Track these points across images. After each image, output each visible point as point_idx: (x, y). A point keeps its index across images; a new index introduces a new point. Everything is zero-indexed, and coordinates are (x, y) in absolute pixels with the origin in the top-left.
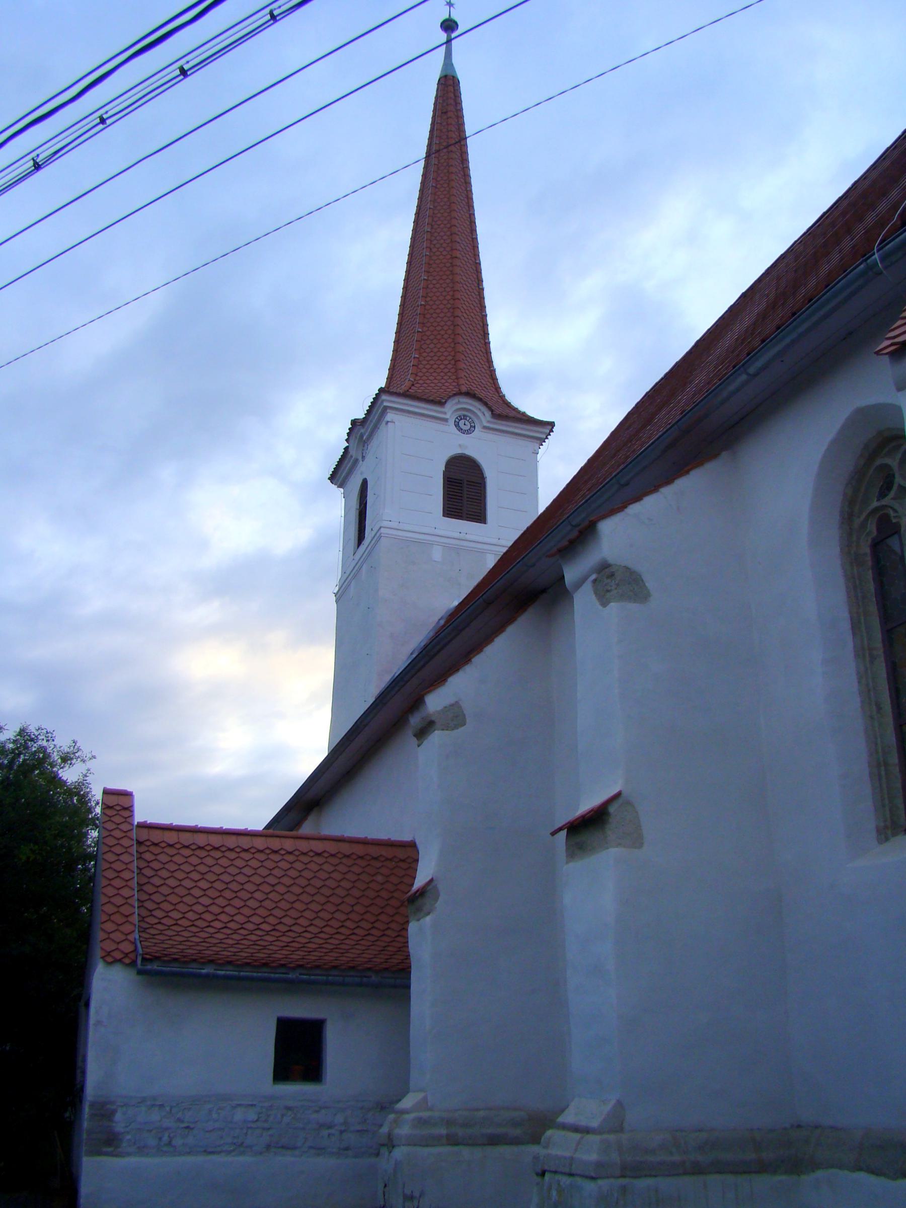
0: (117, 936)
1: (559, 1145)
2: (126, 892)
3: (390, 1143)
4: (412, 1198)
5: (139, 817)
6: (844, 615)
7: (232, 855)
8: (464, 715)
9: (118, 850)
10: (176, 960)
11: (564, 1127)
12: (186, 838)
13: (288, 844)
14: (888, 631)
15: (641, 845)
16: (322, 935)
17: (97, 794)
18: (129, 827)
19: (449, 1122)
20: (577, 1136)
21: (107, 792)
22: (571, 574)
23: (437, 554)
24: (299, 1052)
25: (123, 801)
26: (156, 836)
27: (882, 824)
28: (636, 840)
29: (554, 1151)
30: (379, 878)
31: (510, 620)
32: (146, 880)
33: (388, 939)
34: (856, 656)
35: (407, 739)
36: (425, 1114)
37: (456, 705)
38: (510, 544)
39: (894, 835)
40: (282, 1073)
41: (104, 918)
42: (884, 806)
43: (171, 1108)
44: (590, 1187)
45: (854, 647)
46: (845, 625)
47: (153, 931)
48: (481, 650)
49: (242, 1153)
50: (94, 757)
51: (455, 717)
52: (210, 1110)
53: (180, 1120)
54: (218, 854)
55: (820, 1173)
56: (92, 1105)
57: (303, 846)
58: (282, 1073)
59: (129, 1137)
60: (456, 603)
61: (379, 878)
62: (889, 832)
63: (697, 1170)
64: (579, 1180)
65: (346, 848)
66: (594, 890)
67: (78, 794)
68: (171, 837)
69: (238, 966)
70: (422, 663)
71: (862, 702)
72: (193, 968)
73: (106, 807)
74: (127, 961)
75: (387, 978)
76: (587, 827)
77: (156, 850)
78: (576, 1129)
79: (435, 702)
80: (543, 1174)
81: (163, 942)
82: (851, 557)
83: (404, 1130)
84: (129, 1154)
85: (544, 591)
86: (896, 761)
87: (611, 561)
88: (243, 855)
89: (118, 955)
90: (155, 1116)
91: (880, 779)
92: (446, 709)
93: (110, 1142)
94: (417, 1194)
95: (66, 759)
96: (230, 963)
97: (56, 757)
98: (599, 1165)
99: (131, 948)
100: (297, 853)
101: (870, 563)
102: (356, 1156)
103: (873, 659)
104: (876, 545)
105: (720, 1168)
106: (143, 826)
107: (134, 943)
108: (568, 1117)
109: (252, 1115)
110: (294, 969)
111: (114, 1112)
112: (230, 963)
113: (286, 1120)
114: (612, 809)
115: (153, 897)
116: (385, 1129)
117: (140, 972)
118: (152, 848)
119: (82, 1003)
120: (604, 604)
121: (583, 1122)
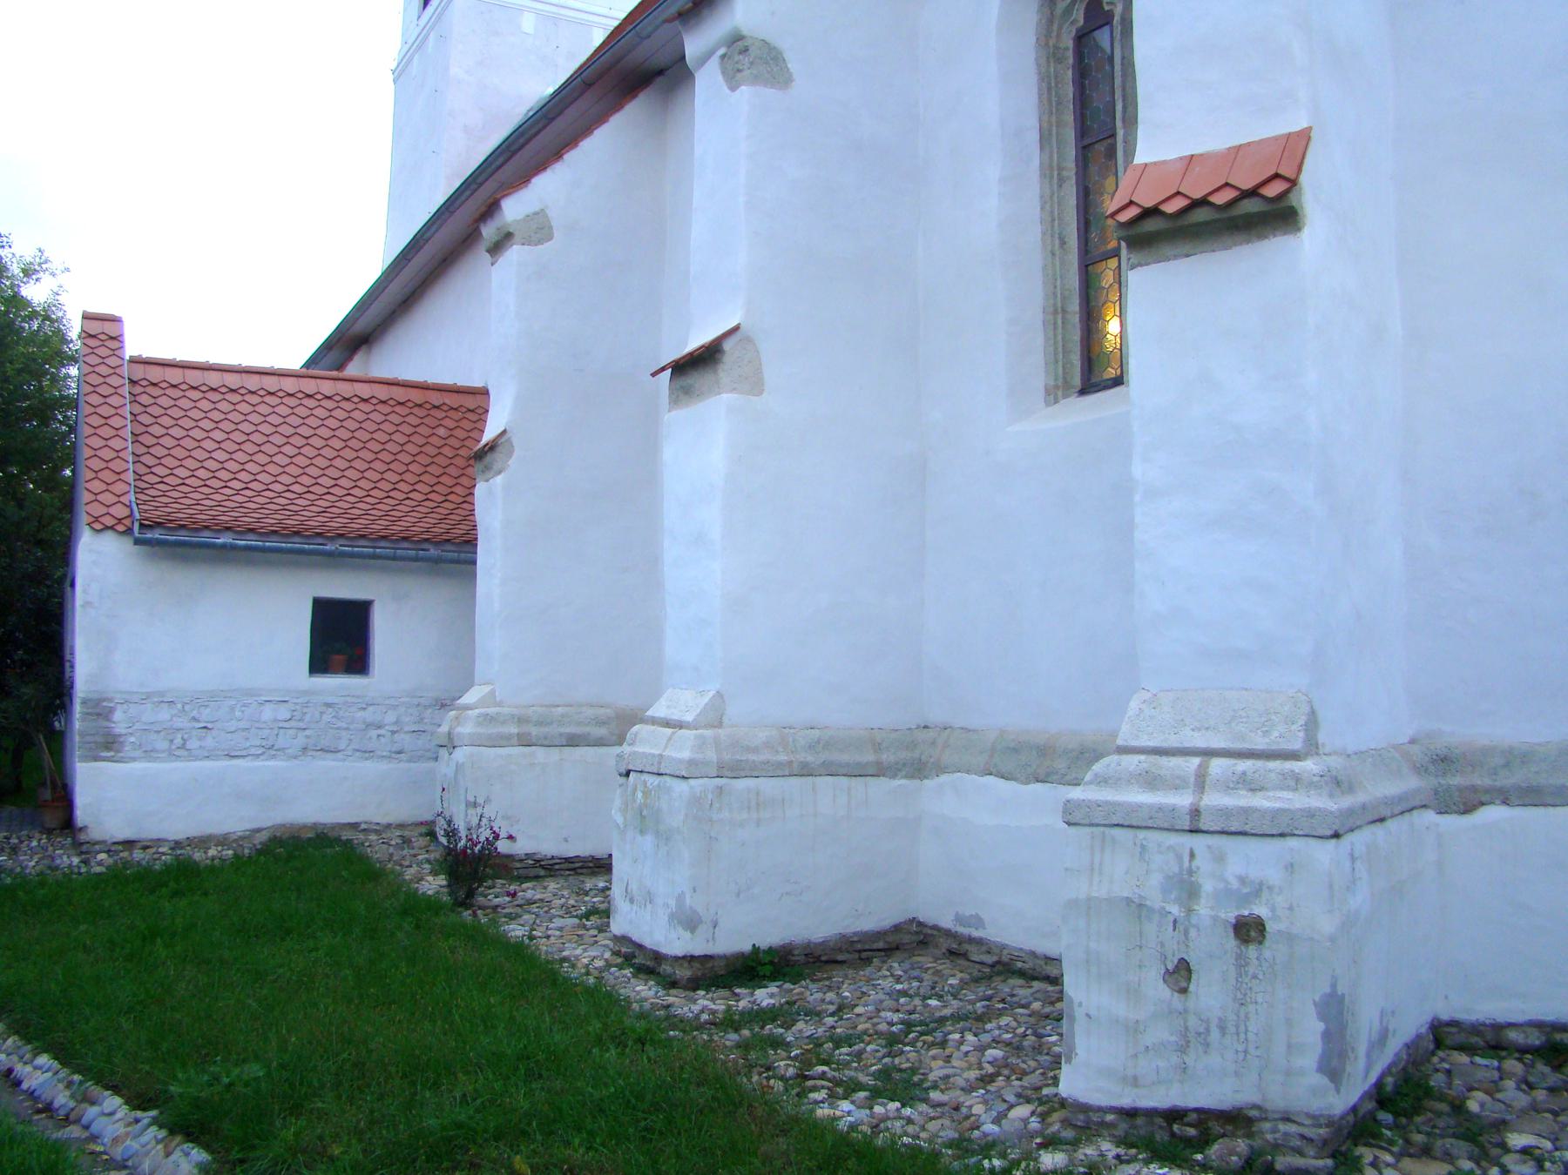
0: (108, 498)
1: (646, 743)
2: (117, 444)
3: (450, 744)
4: (475, 805)
5: (132, 348)
6: (1031, 122)
7: (254, 399)
8: (551, 228)
9: (104, 390)
10: (183, 526)
11: (654, 721)
12: (194, 378)
13: (327, 387)
14: (1084, 148)
15: (761, 393)
16: (368, 499)
17: (74, 329)
18: (119, 362)
19: (521, 720)
20: (669, 731)
21: (87, 317)
22: (694, 45)
23: (528, 23)
24: (340, 638)
25: (109, 328)
26: (155, 374)
27: (1052, 383)
28: (755, 385)
29: (639, 749)
30: (442, 432)
31: (617, 107)
32: (144, 429)
33: (452, 506)
34: (1043, 175)
35: (480, 256)
36: (492, 710)
37: (540, 214)
38: (623, 15)
39: (1065, 396)
40: (319, 664)
41: (91, 475)
42: (1057, 362)
43: (184, 704)
44: (681, 787)
45: (1041, 163)
46: (1033, 137)
47: (152, 492)
48: (576, 145)
49: (274, 757)
50: (68, 270)
51: (539, 229)
52: (232, 709)
53: (195, 719)
54: (235, 398)
55: (944, 778)
56: (84, 702)
57: (346, 389)
58: (319, 664)
59: (132, 739)
60: (551, 90)
61: (442, 432)
62: (1060, 393)
63: (806, 771)
64: (667, 779)
65: (399, 394)
66: (702, 443)
67: (47, 318)
68: (175, 376)
69: (261, 534)
70: (501, 160)
71: (1044, 234)
72: (205, 538)
73: (86, 335)
74: (121, 528)
75: (449, 550)
76: (697, 364)
77: (156, 392)
78: (667, 723)
79: (514, 209)
80: (627, 774)
81: (166, 505)
82: (1049, 52)
83: (466, 729)
84: (134, 759)
85: (660, 72)
86: (1077, 308)
87: (745, 32)
88: (268, 399)
89: (109, 521)
90: (164, 714)
91: (1055, 328)
92: (529, 218)
93: (109, 745)
94: (480, 800)
95: (28, 272)
96: (252, 530)
97: (15, 269)
98: (692, 763)
99: (126, 512)
100: (337, 398)
101: (1071, 61)
102: (409, 761)
103: (1061, 181)
104: (1082, 38)
105: (831, 770)
106: (135, 361)
107: (129, 506)
108: (659, 710)
109: (284, 712)
110: (331, 539)
111: (112, 710)
112: (252, 530)
113: (326, 718)
114: (727, 345)
115: (152, 450)
116: (444, 729)
117: (137, 542)
118: (150, 390)
119: (68, 583)
120: (733, 89)
121: (675, 715)
